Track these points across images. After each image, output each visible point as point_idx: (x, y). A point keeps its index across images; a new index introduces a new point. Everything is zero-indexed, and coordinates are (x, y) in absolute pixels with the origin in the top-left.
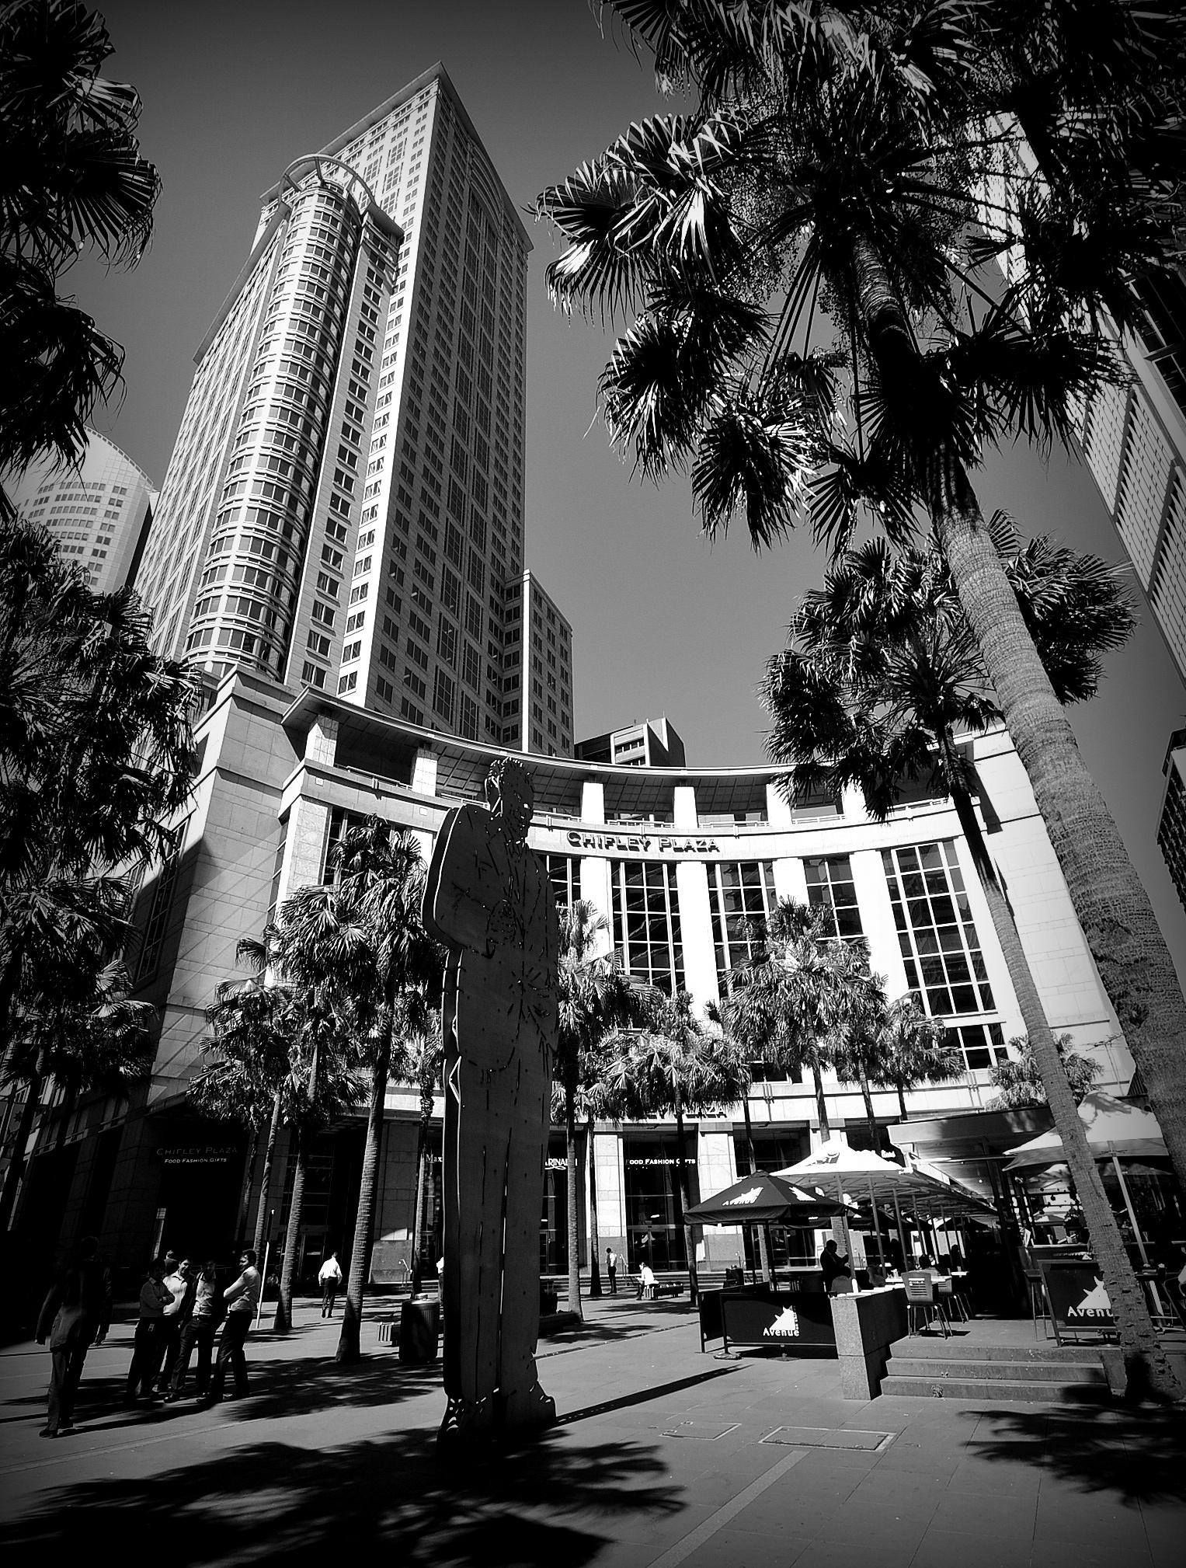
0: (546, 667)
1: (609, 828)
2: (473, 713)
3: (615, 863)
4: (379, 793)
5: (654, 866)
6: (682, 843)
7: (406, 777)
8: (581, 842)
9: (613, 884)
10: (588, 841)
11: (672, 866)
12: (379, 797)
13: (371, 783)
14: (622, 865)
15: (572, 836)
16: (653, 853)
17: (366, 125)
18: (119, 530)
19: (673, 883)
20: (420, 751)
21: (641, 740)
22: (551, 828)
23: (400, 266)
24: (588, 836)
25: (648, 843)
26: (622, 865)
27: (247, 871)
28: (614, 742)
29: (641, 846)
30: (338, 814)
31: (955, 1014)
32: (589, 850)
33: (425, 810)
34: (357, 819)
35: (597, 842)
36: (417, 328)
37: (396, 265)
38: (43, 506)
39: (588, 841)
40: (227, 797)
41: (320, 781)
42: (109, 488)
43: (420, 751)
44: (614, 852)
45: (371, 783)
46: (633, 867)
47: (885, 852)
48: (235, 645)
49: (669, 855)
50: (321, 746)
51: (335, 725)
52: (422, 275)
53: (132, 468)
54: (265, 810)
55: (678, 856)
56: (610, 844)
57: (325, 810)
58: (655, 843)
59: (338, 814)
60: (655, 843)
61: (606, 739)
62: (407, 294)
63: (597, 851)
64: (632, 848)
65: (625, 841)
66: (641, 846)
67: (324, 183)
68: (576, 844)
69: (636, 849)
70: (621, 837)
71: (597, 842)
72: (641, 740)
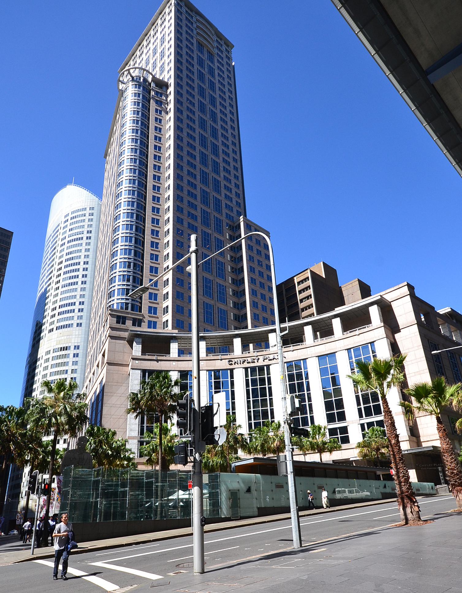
0: (256, 257)
1: (244, 355)
2: (223, 290)
3: (246, 369)
4: (157, 361)
5: (261, 369)
6: (271, 357)
7: (168, 352)
8: (233, 363)
9: (246, 377)
10: (235, 362)
11: (268, 366)
12: (158, 362)
13: (154, 358)
14: (249, 369)
15: (229, 361)
16: (261, 363)
17: (150, 26)
18: (94, 226)
19: (269, 373)
20: (171, 341)
21: (308, 278)
22: (221, 360)
23: (168, 101)
24: (236, 360)
25: (259, 359)
26: (249, 369)
27: (120, 395)
28: (296, 280)
29: (256, 361)
30: (144, 372)
31: (374, 416)
32: (236, 366)
33: (174, 363)
34: (151, 372)
35: (239, 362)
36: (178, 128)
37: (167, 100)
38: (67, 223)
39: (235, 362)
40: (111, 371)
41: (137, 362)
42: (88, 209)
43: (171, 341)
44: (246, 365)
45: (154, 358)
46: (253, 369)
47: (348, 350)
48: (123, 295)
49: (267, 362)
50: (137, 349)
51: (140, 340)
52: (178, 102)
53: (95, 197)
54: (124, 373)
55: (270, 362)
56: (244, 362)
57: (139, 371)
58: (261, 358)
59: (144, 372)
60: (261, 358)
61: (292, 279)
62: (171, 115)
63: (239, 366)
64: (252, 362)
65: (250, 360)
66: (256, 361)
67: (133, 78)
68: (231, 364)
69: (254, 362)
70: (248, 358)
71: (239, 362)
72: (308, 278)
